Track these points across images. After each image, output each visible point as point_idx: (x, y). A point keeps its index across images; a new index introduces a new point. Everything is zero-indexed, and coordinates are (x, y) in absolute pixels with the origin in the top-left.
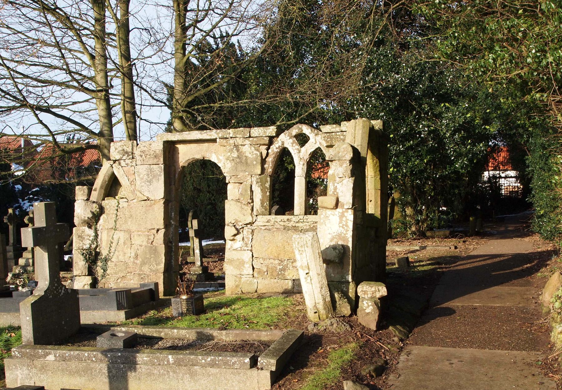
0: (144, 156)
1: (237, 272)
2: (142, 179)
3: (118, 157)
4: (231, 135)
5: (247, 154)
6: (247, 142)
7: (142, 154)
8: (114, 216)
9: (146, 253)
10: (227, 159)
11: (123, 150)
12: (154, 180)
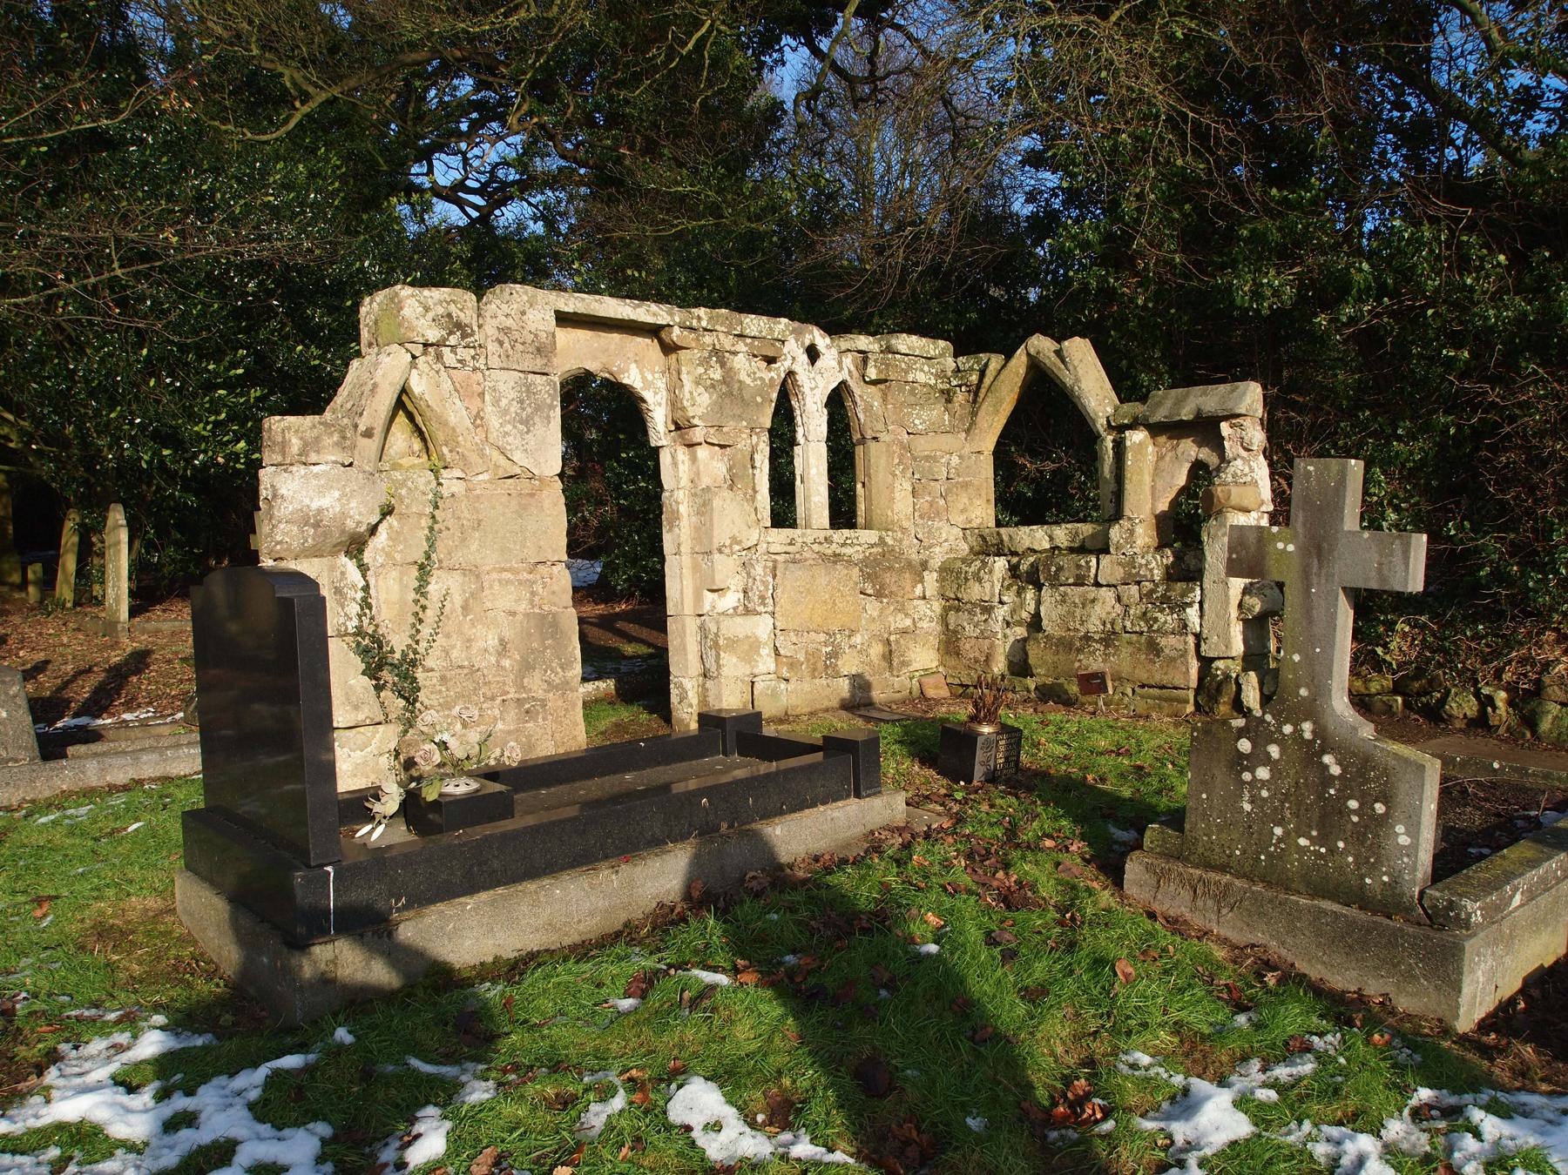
0: (506, 345)
1: (743, 670)
2: (505, 412)
3: (433, 335)
4: (704, 324)
5: (743, 376)
6: (741, 346)
7: (502, 337)
8: (425, 522)
9: (529, 635)
10: (697, 383)
11: (449, 315)
12: (537, 419)
